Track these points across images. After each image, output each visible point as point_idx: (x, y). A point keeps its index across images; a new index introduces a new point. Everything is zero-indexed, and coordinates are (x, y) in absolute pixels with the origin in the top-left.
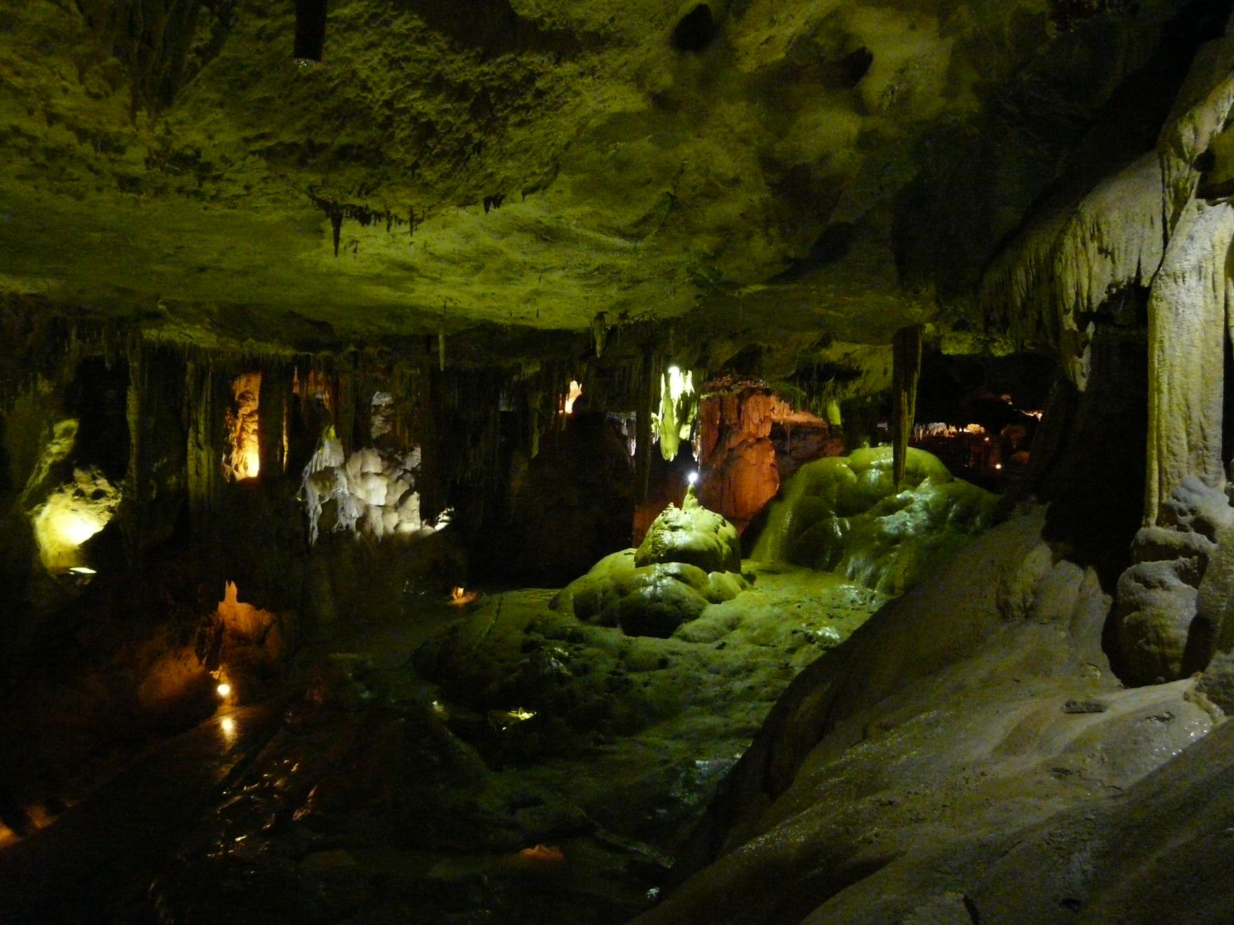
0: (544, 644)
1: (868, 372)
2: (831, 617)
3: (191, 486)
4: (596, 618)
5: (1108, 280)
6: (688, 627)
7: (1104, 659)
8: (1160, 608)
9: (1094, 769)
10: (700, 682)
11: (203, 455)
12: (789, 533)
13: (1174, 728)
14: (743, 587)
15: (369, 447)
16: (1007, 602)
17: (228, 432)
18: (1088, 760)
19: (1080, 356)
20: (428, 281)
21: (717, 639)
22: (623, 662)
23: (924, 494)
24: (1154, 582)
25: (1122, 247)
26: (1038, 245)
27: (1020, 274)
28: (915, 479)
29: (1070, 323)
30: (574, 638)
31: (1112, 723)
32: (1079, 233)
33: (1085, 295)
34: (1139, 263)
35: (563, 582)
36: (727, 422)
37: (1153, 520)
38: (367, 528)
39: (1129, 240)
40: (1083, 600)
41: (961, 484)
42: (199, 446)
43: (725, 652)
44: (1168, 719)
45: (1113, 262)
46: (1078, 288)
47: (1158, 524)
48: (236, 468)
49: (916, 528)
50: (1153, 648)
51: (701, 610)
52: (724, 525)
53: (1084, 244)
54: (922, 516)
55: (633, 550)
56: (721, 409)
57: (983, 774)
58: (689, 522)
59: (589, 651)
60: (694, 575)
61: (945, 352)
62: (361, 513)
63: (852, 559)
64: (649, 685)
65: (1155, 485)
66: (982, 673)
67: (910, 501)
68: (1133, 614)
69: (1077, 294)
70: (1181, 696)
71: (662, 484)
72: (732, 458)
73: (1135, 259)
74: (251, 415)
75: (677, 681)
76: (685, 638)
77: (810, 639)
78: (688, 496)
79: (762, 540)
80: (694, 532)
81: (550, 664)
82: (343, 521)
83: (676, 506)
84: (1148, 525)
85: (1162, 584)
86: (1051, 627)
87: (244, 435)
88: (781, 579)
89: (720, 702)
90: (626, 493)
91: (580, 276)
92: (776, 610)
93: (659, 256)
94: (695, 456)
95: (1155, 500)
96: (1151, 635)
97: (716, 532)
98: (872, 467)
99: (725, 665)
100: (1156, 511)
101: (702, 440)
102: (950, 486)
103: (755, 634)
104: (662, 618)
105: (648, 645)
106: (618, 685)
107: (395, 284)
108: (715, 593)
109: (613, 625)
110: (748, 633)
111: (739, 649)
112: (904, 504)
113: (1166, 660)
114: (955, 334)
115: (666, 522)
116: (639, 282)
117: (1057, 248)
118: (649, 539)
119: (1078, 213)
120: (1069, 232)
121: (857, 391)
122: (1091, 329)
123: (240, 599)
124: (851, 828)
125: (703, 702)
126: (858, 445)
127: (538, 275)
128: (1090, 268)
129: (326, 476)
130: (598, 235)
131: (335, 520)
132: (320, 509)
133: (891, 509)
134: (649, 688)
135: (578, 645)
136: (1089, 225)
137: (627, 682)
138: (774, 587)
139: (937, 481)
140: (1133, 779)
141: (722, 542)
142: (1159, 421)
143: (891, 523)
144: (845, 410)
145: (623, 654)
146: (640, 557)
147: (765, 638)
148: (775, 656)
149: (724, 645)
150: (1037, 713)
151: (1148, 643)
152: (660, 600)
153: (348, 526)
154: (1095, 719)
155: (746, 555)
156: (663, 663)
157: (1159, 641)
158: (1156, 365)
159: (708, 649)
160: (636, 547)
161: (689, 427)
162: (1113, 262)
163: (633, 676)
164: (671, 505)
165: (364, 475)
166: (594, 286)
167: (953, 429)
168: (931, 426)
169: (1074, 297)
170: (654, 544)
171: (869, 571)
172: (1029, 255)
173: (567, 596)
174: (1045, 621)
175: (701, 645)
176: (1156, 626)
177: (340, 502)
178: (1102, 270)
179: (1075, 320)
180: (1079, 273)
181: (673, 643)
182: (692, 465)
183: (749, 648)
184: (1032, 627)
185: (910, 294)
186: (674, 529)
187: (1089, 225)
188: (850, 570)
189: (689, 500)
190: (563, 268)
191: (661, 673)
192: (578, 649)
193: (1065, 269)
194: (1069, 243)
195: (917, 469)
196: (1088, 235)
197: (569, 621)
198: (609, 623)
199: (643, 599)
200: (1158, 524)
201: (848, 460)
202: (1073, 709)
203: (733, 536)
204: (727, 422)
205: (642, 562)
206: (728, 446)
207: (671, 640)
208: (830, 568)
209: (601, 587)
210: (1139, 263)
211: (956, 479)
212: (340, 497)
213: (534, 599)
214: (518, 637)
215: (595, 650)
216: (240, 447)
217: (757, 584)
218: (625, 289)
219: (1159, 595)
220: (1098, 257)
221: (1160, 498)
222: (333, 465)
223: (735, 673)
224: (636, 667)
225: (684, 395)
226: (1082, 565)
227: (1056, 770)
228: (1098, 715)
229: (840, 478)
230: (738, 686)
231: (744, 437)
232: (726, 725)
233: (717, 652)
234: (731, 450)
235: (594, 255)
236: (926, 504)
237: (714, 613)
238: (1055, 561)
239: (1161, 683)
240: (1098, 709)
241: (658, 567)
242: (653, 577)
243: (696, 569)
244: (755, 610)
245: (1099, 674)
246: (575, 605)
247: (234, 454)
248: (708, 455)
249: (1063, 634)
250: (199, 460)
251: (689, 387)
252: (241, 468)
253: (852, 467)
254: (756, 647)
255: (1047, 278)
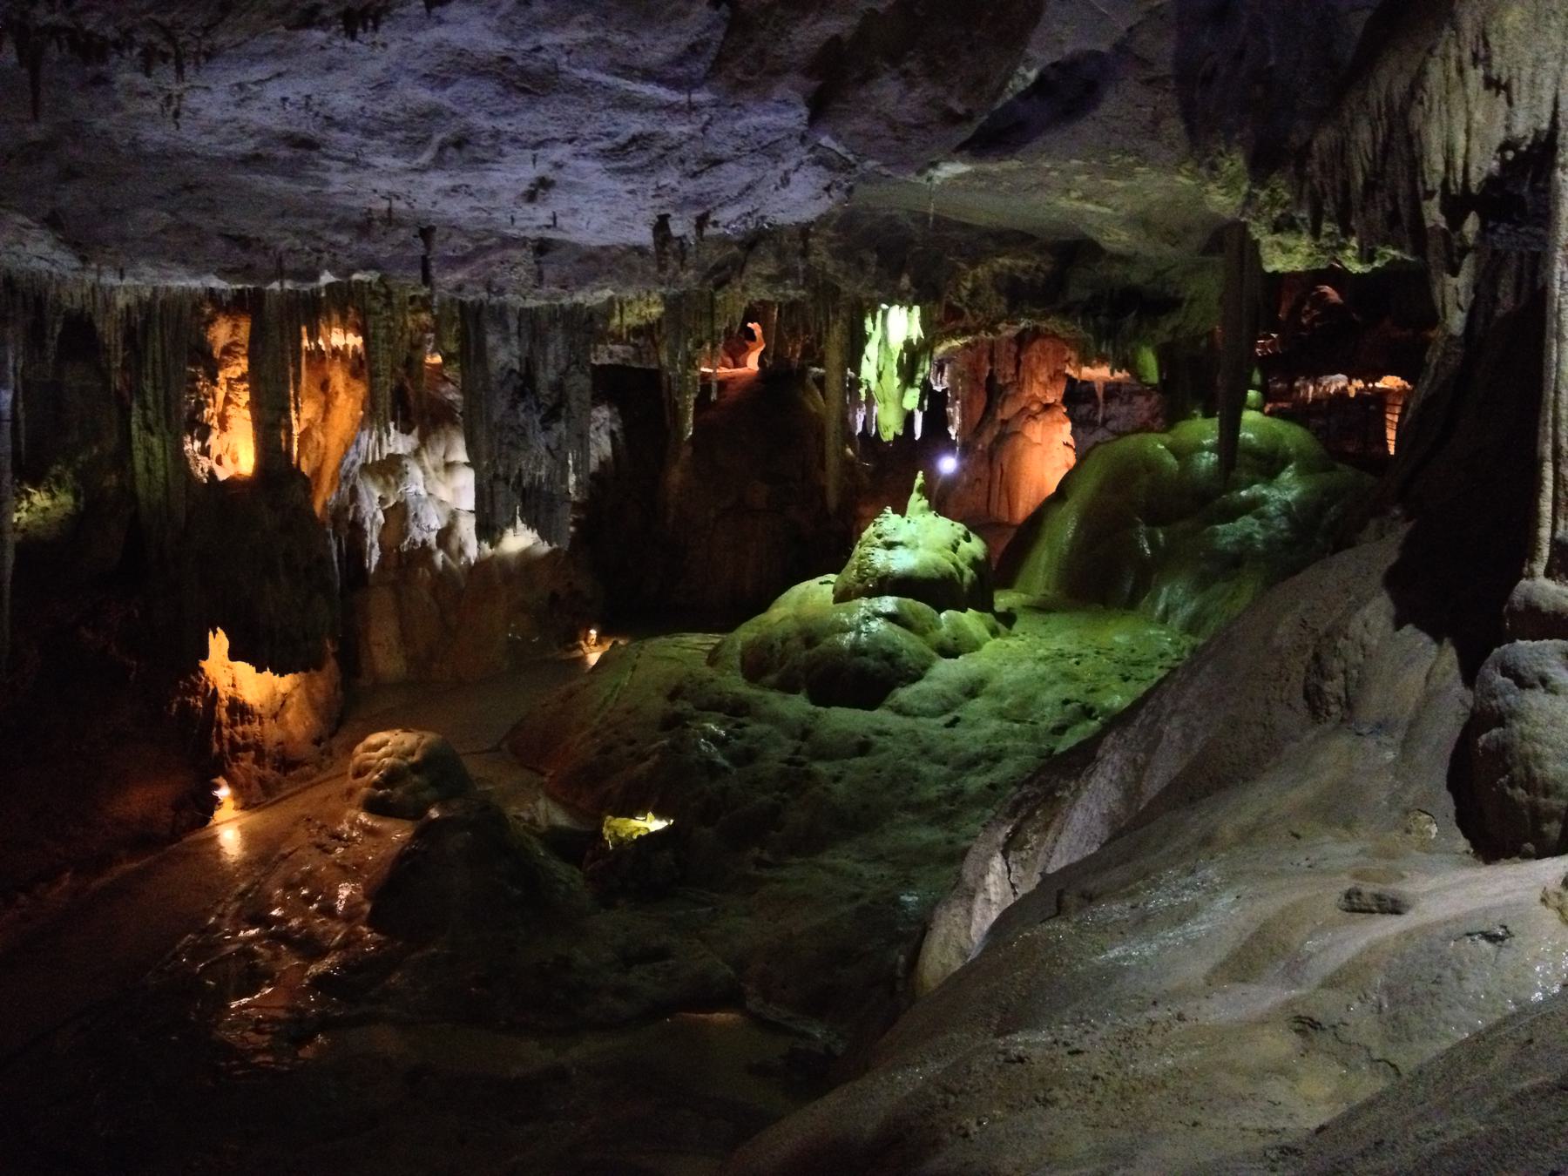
0: (692, 718)
1: (1192, 300)
2: (1126, 679)
3: (141, 489)
4: (772, 678)
5: (1499, 135)
6: (904, 694)
7: (1447, 803)
8: (1536, 724)
9: (1362, 1023)
10: (917, 776)
11: (155, 441)
12: (1071, 551)
13: (1507, 956)
14: (994, 633)
15: (454, 423)
16: (1319, 689)
17: (201, 406)
18: (1357, 1004)
19: (1455, 273)
20: (342, 165)
21: (946, 711)
22: (806, 746)
23: (1287, 489)
24: (1529, 676)
25: (1527, 72)
26: (1389, 81)
27: (1363, 134)
28: (1269, 463)
29: (1433, 214)
30: (737, 709)
31: (1409, 935)
32: (1453, 51)
33: (1460, 162)
34: (1556, 104)
35: (728, 624)
36: (1000, 382)
37: (1540, 568)
38: (454, 546)
39: (1538, 62)
40: (1430, 697)
41: (1346, 472)
42: (148, 428)
43: (958, 731)
44: (1502, 939)
45: (1510, 102)
46: (1449, 151)
47: (1548, 574)
48: (219, 461)
49: (1268, 542)
50: (1519, 794)
51: (925, 668)
52: (968, 539)
53: (1461, 71)
54: (1282, 524)
55: (832, 577)
56: (991, 360)
57: (1180, 1017)
58: (915, 537)
59: (755, 728)
60: (917, 615)
61: (1269, 269)
62: (445, 522)
63: (1165, 590)
64: (840, 781)
65: (1546, 507)
66: (1247, 818)
67: (1264, 500)
68: (1495, 732)
69: (1449, 164)
70: (1538, 895)
71: (890, 471)
72: (1007, 435)
73: (1548, 96)
74: (240, 379)
75: (883, 774)
76: (900, 710)
77: (1087, 712)
78: (915, 496)
79: (1034, 555)
80: (921, 550)
81: (697, 746)
82: (416, 534)
83: (894, 512)
84: (1532, 575)
85: (1544, 681)
86: (1370, 743)
87: (231, 410)
88: (1055, 619)
89: (946, 807)
90: (814, 490)
91: (604, 155)
92: (1042, 668)
93: (740, 117)
94: (952, 431)
95: (1545, 532)
96: (1518, 771)
97: (955, 549)
98: (1202, 448)
99: (956, 750)
100: (1546, 551)
101: (962, 410)
102: (1325, 476)
103: (1005, 704)
104: (869, 678)
105: (845, 719)
106: (796, 778)
107: (293, 171)
108: (950, 642)
109: (794, 690)
110: (995, 704)
111: (981, 725)
112: (1253, 506)
113: (1538, 816)
114: (1278, 237)
115: (879, 536)
116: (718, 162)
117: (1418, 81)
118: (854, 561)
119: (1452, 14)
120: (1437, 52)
121: (1175, 329)
122: (1471, 225)
123: (234, 655)
124: (952, 1099)
125: (919, 807)
126: (1186, 415)
127: (529, 153)
128: (1469, 113)
129: (390, 469)
130: (621, 81)
131: (404, 533)
132: (381, 517)
133: (1232, 513)
134: (840, 786)
135: (741, 720)
136: (1469, 35)
137: (809, 775)
138: (1042, 631)
139: (1305, 470)
140: (1430, 1050)
141: (962, 565)
142: (1557, 392)
143: (1228, 533)
144: (1166, 357)
145: (806, 734)
146: (840, 586)
147: (1021, 710)
148: (1035, 738)
149: (957, 720)
150: (1295, 907)
151: (1512, 784)
152: (865, 653)
153: (424, 542)
154: (1386, 928)
155: (1007, 583)
156: (864, 748)
157: (1530, 784)
158: (1558, 291)
159: (932, 727)
160: (837, 571)
161: (917, 392)
162: (1510, 102)
163: (820, 767)
164: (889, 510)
165: (449, 467)
166: (633, 170)
167: (1359, 384)
168: (1325, 381)
169: (1441, 167)
170: (860, 569)
171: (1191, 607)
172: (1375, 96)
173: (733, 646)
174: (1365, 730)
175: (922, 720)
176: (1527, 756)
177: (411, 507)
178: (1490, 117)
179: (1443, 210)
180: (1450, 127)
181: (882, 717)
182: (949, 446)
183: (995, 724)
184: (1343, 742)
185: (1203, 171)
186: (890, 546)
187: (1469, 35)
188: (1161, 607)
189: (916, 502)
190: (570, 141)
191: (859, 761)
192: (740, 726)
193: (1427, 117)
194: (1435, 72)
195: (1275, 452)
196: (1467, 55)
197: (735, 684)
198: (788, 686)
199: (840, 651)
200: (1548, 574)
201: (1167, 438)
202: (1354, 905)
203: (980, 555)
204: (1000, 382)
205: (843, 596)
206: (1000, 417)
207: (879, 713)
208: (1131, 604)
209: (780, 633)
210: (1556, 104)
211: (1339, 466)
212: (411, 499)
213: (691, 647)
214: (657, 705)
215: (766, 727)
216: (223, 427)
217: (1016, 628)
218: (694, 175)
219: (1536, 699)
220: (1485, 94)
221: (1554, 529)
222: (401, 451)
223: (971, 763)
224: (824, 753)
225: (908, 344)
226: (1438, 639)
227: (1299, 1019)
228: (1394, 918)
229: (1151, 465)
230: (974, 782)
231: (1023, 403)
232: (950, 842)
233: (945, 731)
234: (1005, 422)
235: (623, 118)
236: (1288, 504)
237: (947, 671)
238: (1399, 624)
239: (1527, 856)
240: (1394, 907)
241: (864, 605)
242: (856, 617)
243: (921, 605)
244: (1009, 667)
245: (1434, 829)
246: (743, 661)
247: (212, 440)
248: (973, 430)
249: (1390, 756)
250: (149, 450)
251: (916, 332)
252: (226, 460)
253: (1172, 449)
254: (1006, 724)
255: (1401, 144)
